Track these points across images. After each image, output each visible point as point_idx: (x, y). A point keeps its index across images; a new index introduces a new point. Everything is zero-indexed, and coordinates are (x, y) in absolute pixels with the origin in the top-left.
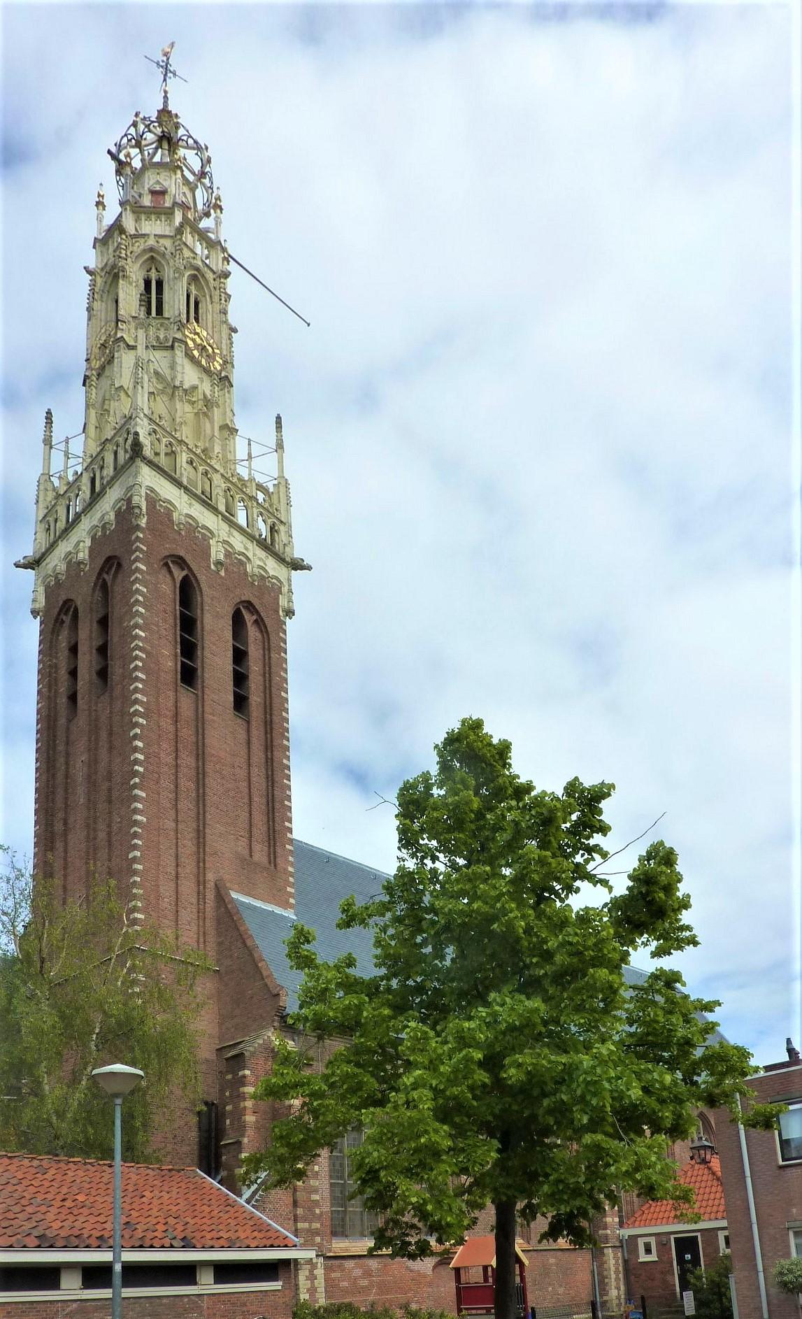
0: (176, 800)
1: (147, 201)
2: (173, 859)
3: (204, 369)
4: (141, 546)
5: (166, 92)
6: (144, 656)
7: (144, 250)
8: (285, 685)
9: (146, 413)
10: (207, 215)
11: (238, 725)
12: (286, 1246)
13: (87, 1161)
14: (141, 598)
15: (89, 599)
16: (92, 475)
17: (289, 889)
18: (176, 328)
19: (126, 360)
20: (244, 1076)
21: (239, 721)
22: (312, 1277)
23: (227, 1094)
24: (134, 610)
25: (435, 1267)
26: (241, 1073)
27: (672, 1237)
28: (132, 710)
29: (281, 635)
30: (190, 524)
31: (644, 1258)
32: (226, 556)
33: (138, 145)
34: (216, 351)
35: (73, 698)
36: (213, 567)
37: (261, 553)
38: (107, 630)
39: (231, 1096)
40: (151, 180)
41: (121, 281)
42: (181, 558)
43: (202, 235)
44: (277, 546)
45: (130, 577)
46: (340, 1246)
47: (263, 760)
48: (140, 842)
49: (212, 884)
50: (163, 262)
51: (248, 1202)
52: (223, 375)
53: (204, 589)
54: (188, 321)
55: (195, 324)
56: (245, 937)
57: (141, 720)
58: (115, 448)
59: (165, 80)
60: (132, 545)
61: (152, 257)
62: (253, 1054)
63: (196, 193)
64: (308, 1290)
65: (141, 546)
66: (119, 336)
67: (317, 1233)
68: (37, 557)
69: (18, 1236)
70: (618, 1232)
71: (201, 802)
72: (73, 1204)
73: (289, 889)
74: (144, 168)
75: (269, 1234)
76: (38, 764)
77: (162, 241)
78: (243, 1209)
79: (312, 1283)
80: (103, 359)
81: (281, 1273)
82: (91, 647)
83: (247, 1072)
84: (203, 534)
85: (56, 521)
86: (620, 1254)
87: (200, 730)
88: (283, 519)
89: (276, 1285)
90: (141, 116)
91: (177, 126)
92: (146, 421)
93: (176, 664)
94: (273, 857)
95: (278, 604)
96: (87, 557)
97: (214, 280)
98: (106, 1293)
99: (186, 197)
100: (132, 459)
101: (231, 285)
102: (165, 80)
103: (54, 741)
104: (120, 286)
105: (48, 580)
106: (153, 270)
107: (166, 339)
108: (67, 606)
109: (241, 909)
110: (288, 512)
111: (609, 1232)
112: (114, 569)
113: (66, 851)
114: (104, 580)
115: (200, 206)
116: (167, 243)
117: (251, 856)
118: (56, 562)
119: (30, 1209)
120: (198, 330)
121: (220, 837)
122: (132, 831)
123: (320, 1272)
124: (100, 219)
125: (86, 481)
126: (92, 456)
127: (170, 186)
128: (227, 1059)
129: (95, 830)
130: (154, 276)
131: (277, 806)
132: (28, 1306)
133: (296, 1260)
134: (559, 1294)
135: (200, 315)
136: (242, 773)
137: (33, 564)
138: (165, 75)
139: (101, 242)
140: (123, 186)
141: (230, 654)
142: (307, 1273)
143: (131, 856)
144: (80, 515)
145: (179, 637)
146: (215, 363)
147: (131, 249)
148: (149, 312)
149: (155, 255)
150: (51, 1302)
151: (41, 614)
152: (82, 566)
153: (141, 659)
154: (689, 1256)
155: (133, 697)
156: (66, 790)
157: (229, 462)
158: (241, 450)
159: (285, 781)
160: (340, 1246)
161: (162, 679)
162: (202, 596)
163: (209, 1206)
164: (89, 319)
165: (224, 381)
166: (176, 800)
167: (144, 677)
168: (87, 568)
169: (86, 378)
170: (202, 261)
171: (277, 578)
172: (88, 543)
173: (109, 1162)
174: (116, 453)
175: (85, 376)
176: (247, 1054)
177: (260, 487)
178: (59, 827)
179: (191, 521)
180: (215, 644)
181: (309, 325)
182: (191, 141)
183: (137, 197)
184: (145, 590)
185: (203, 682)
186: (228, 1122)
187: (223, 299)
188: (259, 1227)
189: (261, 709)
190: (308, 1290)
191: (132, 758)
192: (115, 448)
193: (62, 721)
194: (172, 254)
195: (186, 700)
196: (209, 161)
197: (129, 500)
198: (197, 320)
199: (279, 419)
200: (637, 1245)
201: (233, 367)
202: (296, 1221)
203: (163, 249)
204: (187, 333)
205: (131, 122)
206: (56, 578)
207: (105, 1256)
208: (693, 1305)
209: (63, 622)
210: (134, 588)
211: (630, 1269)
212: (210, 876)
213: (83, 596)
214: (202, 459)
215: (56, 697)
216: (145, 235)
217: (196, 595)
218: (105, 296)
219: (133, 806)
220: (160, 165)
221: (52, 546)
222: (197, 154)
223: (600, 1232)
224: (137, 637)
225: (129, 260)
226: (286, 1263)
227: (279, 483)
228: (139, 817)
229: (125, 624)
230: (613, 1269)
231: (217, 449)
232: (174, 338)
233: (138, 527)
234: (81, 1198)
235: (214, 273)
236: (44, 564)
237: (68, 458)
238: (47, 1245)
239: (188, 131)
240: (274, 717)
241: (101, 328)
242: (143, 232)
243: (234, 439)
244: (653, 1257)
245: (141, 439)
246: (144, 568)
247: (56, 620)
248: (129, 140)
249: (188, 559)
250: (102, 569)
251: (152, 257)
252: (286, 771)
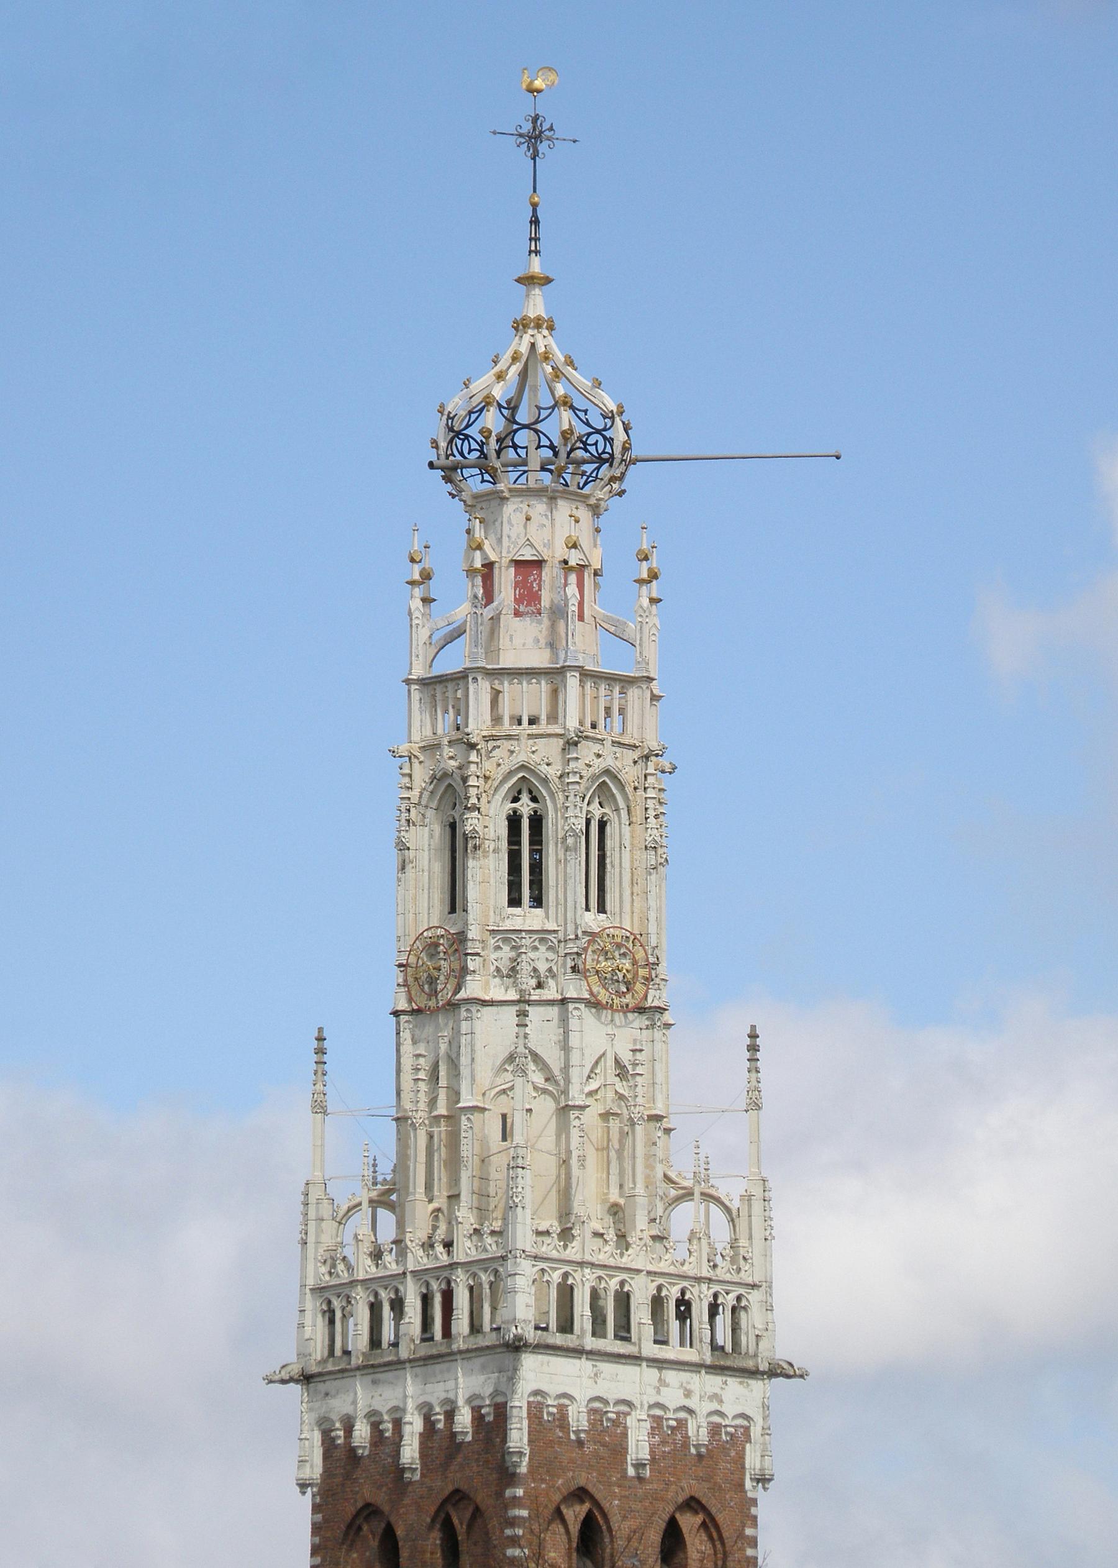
5: (535, 206)
79: (375, 1169)
95: (743, 1467)
96: (417, 1455)
130: (525, 807)
135: (608, 854)
181: (838, 458)
217: (602, 1539)
247: (349, 1526)
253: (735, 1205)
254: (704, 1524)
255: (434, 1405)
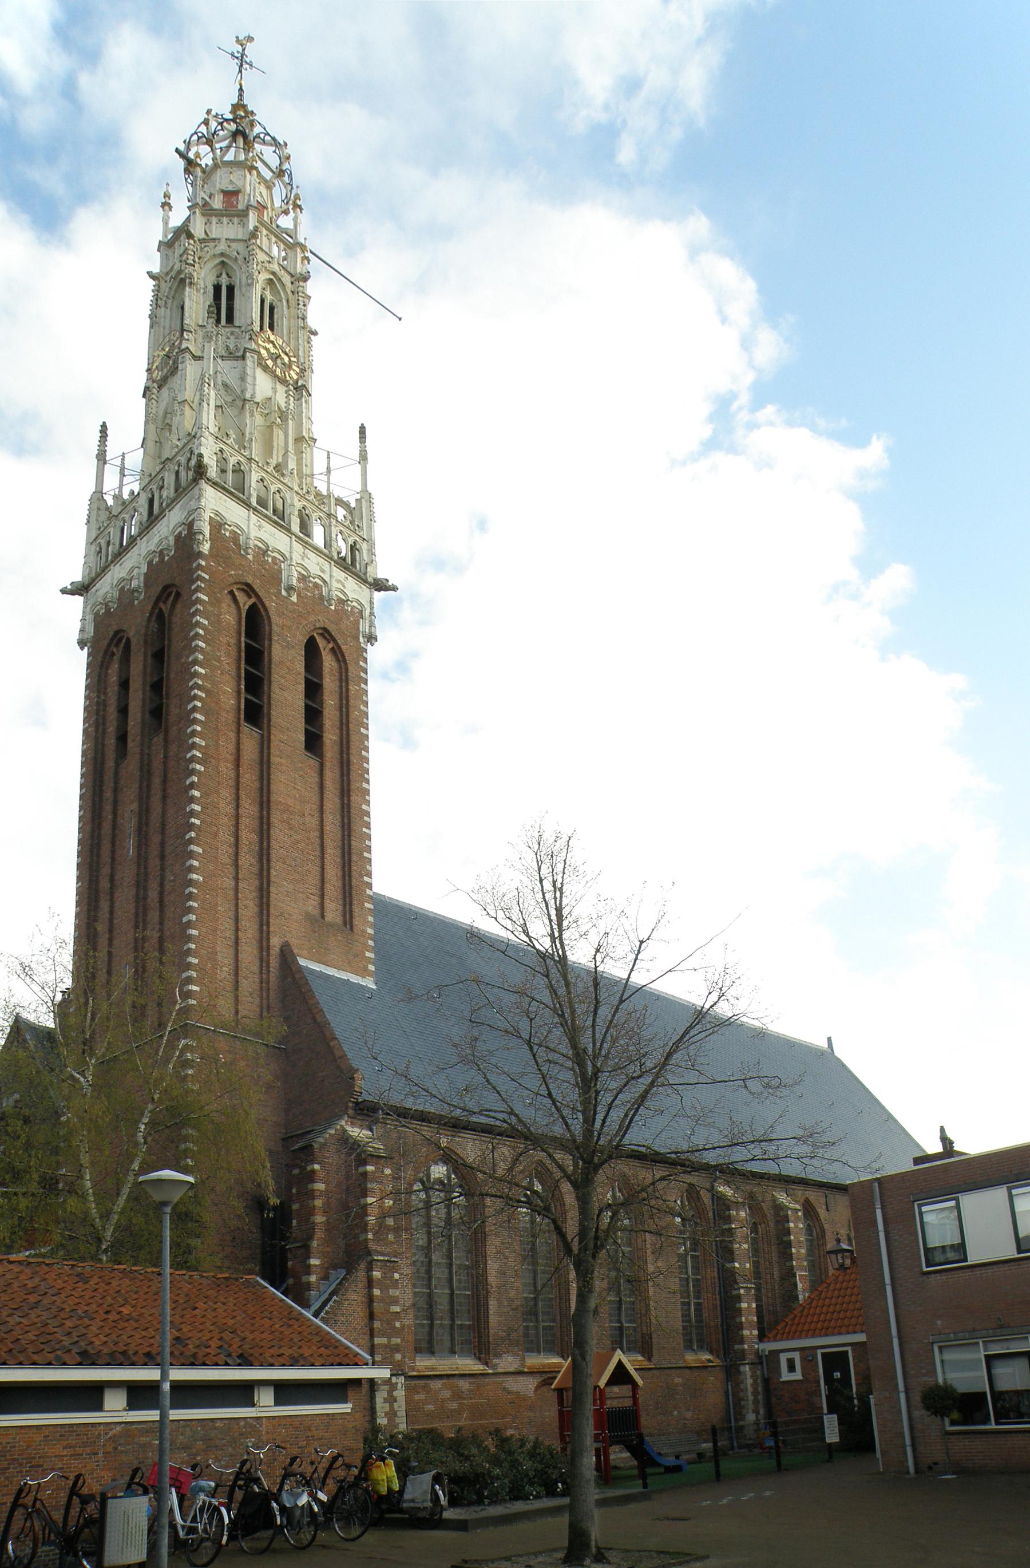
0: (237, 854)
1: (217, 203)
2: (232, 922)
3: (278, 378)
4: (203, 575)
6: (204, 695)
7: (214, 255)
8: (365, 721)
9: (211, 430)
10: (286, 212)
11: (313, 762)
12: (356, 1364)
13: (133, 1268)
14: (201, 632)
15: (143, 631)
16: (150, 496)
17: (368, 954)
18: (248, 337)
19: (190, 369)
20: (313, 1171)
21: (311, 762)
22: (391, 1400)
23: (294, 1191)
24: (193, 644)
25: (537, 1388)
26: (309, 1168)
27: (819, 1352)
28: (189, 755)
29: (361, 663)
30: (259, 548)
31: (786, 1376)
32: (299, 580)
33: (209, 143)
34: (293, 359)
35: (122, 738)
36: (284, 593)
37: (339, 574)
38: (162, 668)
39: (298, 1192)
40: (223, 180)
41: (187, 289)
42: (248, 585)
43: (279, 234)
44: (358, 565)
45: (190, 609)
46: (424, 1363)
47: (338, 806)
48: (195, 905)
49: (278, 950)
50: (235, 267)
51: (316, 1315)
52: (299, 384)
53: (273, 617)
54: (261, 329)
55: (270, 332)
56: (315, 1011)
57: (198, 767)
58: (176, 468)
59: (240, 71)
60: (194, 574)
61: (223, 263)
62: (323, 1146)
63: (273, 191)
64: (386, 1414)
65: (203, 575)
66: (183, 346)
67: (396, 1349)
68: (86, 583)
69: (59, 1353)
70: (756, 1346)
71: (265, 857)
72: (118, 1317)
73: (368, 954)
74: (216, 166)
75: (336, 1351)
76: (82, 812)
77: (234, 245)
78: (309, 1323)
80: (165, 370)
81: (351, 1394)
82: (144, 684)
83: (317, 1167)
84: (274, 558)
85: (108, 543)
86: (758, 1372)
87: (265, 774)
88: (365, 537)
89: (345, 1408)
90: (213, 113)
91: (252, 124)
92: (211, 439)
93: (239, 703)
94: (348, 920)
95: (358, 629)
96: (142, 585)
97: (292, 283)
98: (153, 1415)
99: (262, 196)
100: (195, 481)
101: (311, 287)
102: (240, 71)
103: (101, 786)
104: (187, 294)
105: (98, 607)
106: (224, 275)
107: (237, 349)
108: (118, 637)
109: (309, 978)
110: (370, 528)
111: (746, 1347)
112: (172, 598)
113: (111, 913)
114: (161, 610)
115: (278, 203)
116: (240, 247)
117: (323, 917)
118: (106, 587)
119: (69, 1323)
120: (272, 338)
121: (287, 896)
122: (187, 892)
123: (400, 1393)
124: (166, 222)
125: (143, 501)
126: (150, 475)
127: (244, 186)
128: (293, 1151)
129: (145, 889)
130: (224, 281)
131: (354, 858)
132: (67, 1429)
133: (372, 1381)
134: (686, 1419)
135: (275, 321)
136: (313, 822)
137: (80, 589)
138: (241, 66)
139: (166, 246)
140: (192, 184)
141: (301, 687)
142: (385, 1394)
143: (185, 920)
144: (136, 539)
145: (243, 671)
146: (292, 372)
147: (199, 254)
148: (218, 321)
149: (225, 260)
150: (93, 1425)
151: (88, 644)
152: (136, 594)
153: (200, 699)
154: (839, 1374)
155: (190, 741)
156: (113, 843)
157: (304, 475)
158: (319, 465)
159: (364, 829)
160: (424, 1363)
161: (223, 720)
162: (270, 625)
163: (270, 1319)
164: (151, 327)
165: (300, 390)
166: (237, 854)
167: (203, 718)
168: (142, 597)
169: (147, 389)
170: (279, 264)
171: (358, 601)
172: (144, 569)
173: (157, 1270)
174: (177, 473)
175: (145, 387)
176: (316, 1146)
177: (339, 502)
178: (105, 884)
179: (260, 545)
180: (284, 678)
181: (400, 319)
182: (267, 138)
183: (207, 199)
184: (206, 622)
185: (269, 720)
186: (294, 1222)
187: (301, 303)
188: (327, 1342)
189: (337, 748)
190: (386, 1414)
191: (188, 809)
192: (176, 468)
193: (110, 764)
194: (245, 259)
195: (250, 737)
196: (288, 158)
197: (190, 525)
198: (271, 327)
199: (362, 430)
200: (778, 1362)
201: (312, 371)
202: (372, 1335)
203: (236, 253)
204: (260, 342)
205: (202, 120)
206: (107, 605)
207: (152, 1374)
208: (837, 1430)
209: (113, 654)
210: (194, 620)
211: (768, 1384)
212: (275, 942)
213: (136, 628)
214: (274, 477)
215: (103, 738)
216: (215, 239)
218: (170, 302)
219: (188, 864)
220: (235, 164)
221: (104, 570)
222: (275, 152)
223: (736, 1347)
224: (196, 674)
225: (197, 265)
226: (357, 1382)
227: (362, 498)
228: (195, 876)
229: (183, 660)
230: (750, 1389)
231: (292, 464)
232: (245, 348)
233: (200, 555)
234: (126, 1310)
235: (292, 276)
236: (94, 590)
237: (124, 476)
238: (89, 1362)
239: (265, 129)
240: (352, 757)
241: (164, 337)
242: (214, 236)
243: (312, 450)
244: (798, 1376)
245: (206, 460)
246: (206, 598)
248: (199, 138)
249: (257, 585)
250: (158, 600)
251: (223, 263)
252: (366, 818)
253: (353, 505)
254: (332, 649)
255: (592, 1483)
